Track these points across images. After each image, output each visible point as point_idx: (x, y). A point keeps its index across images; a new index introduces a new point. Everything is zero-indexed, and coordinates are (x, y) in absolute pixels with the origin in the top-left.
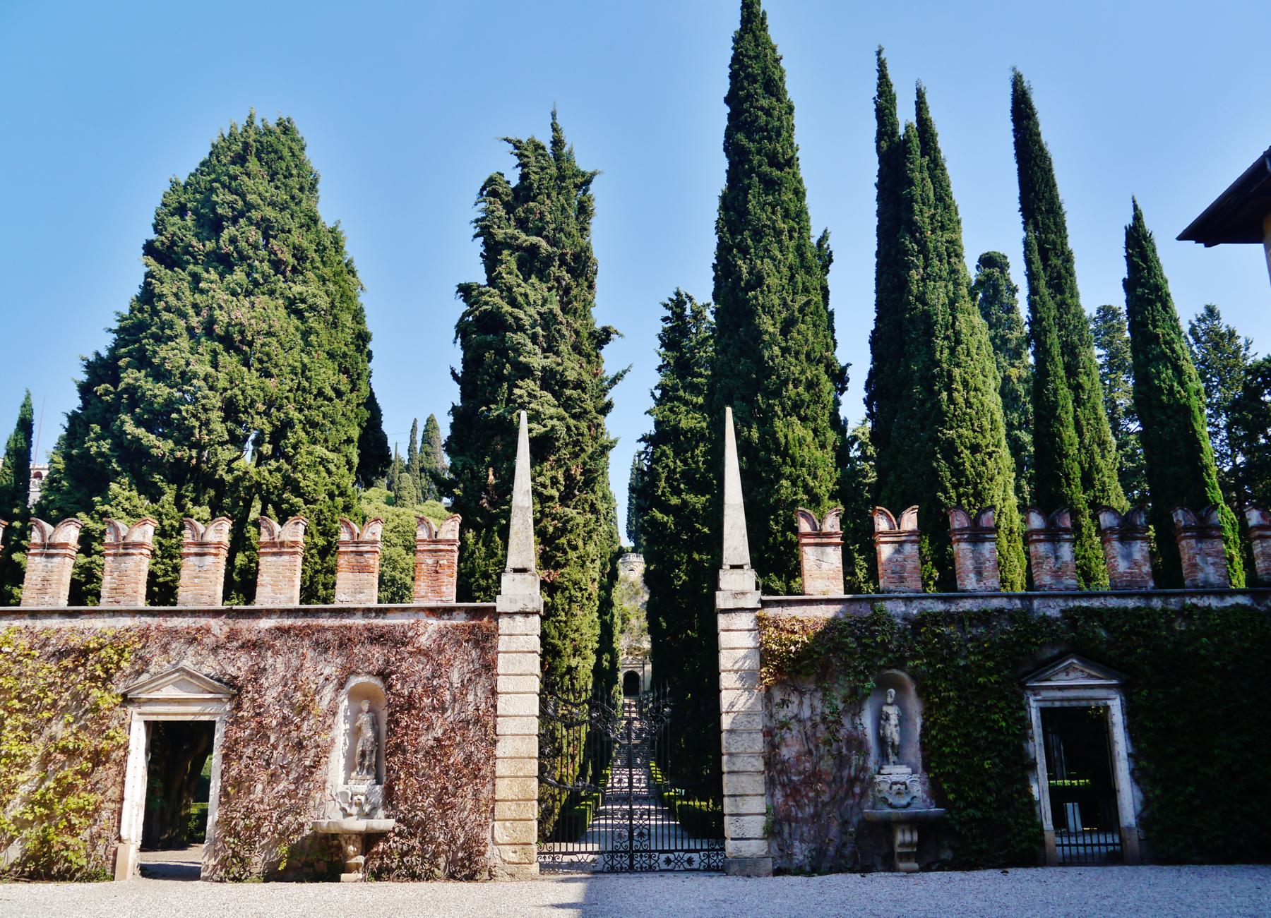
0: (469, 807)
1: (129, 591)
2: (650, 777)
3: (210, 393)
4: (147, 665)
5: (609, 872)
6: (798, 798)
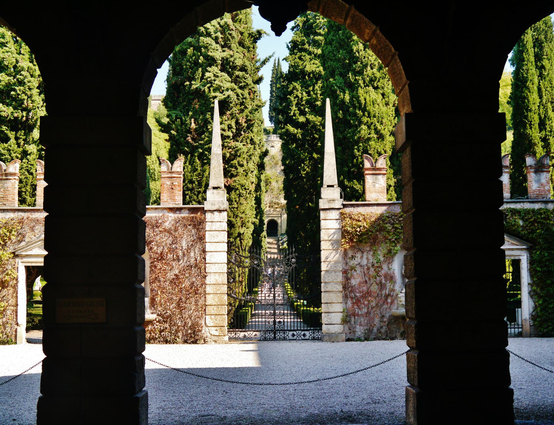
0: (193, 308)
1: (10, 199)
2: (285, 292)
3: (32, 79)
4: (24, 237)
5: (263, 340)
6: (359, 304)
